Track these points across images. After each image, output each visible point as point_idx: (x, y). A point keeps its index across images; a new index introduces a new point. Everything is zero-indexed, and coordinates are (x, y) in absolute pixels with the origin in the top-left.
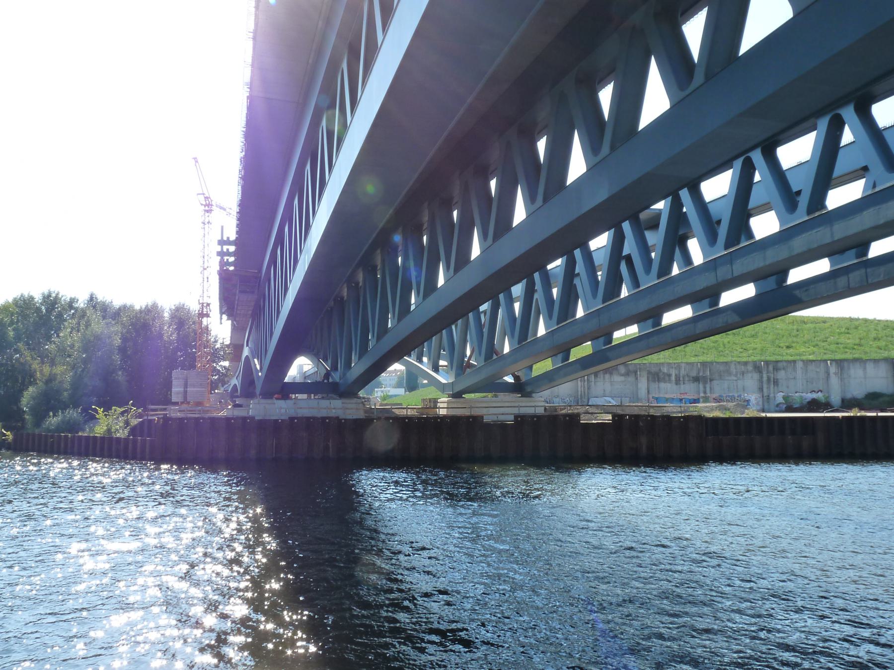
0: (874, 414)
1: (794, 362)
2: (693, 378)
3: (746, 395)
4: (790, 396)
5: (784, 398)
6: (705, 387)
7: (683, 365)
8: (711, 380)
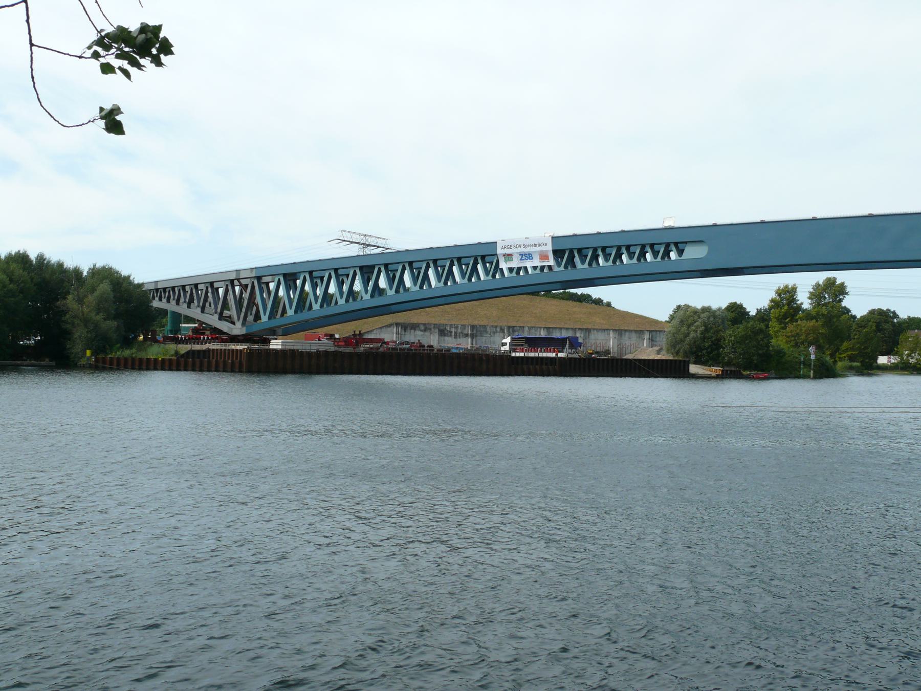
0: (554, 355)
1: (523, 327)
6: (472, 341)
8: (476, 336)
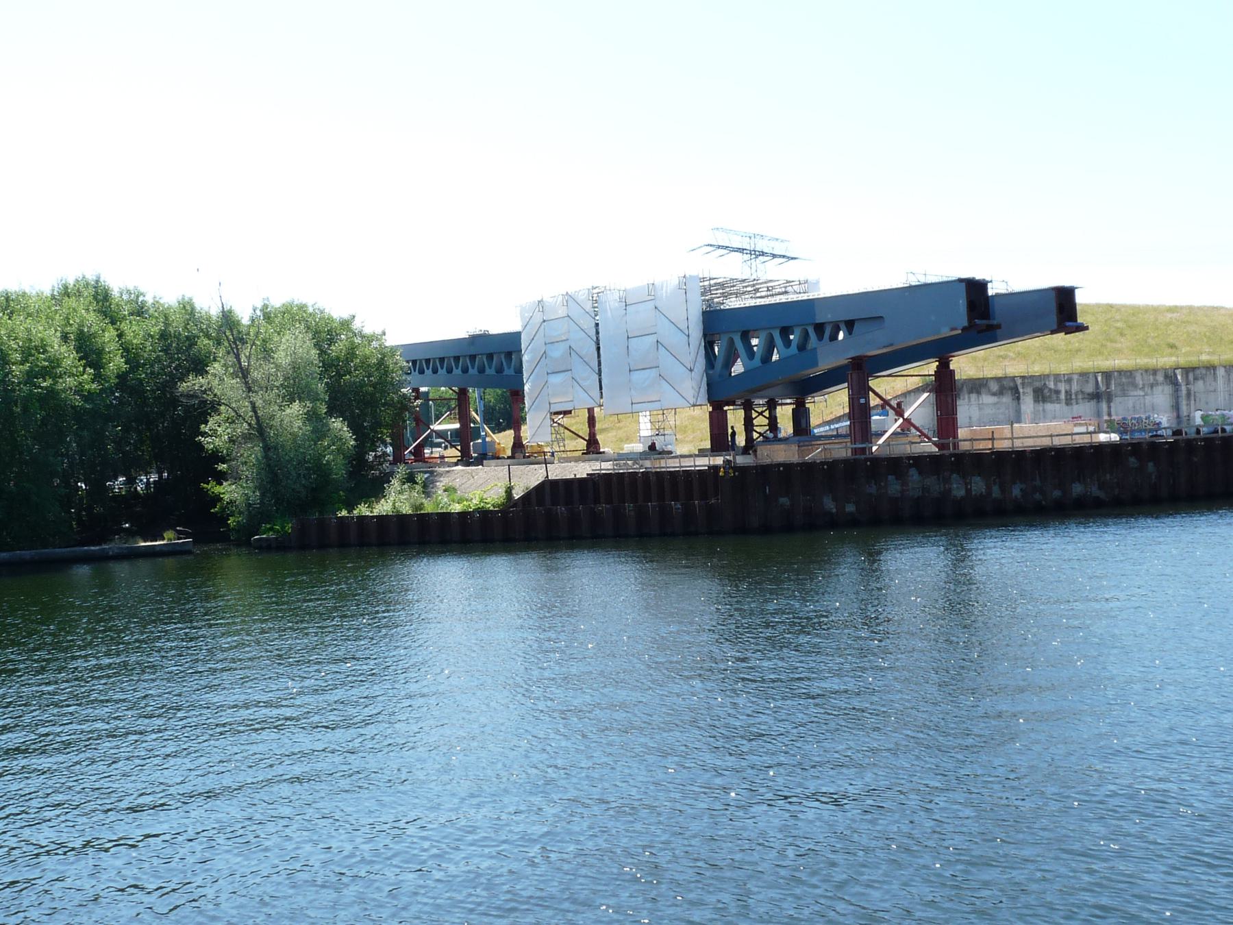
2: (1089, 394)
3: (1156, 416)
4: (1211, 415)
5: (1203, 418)
7: (1075, 377)
